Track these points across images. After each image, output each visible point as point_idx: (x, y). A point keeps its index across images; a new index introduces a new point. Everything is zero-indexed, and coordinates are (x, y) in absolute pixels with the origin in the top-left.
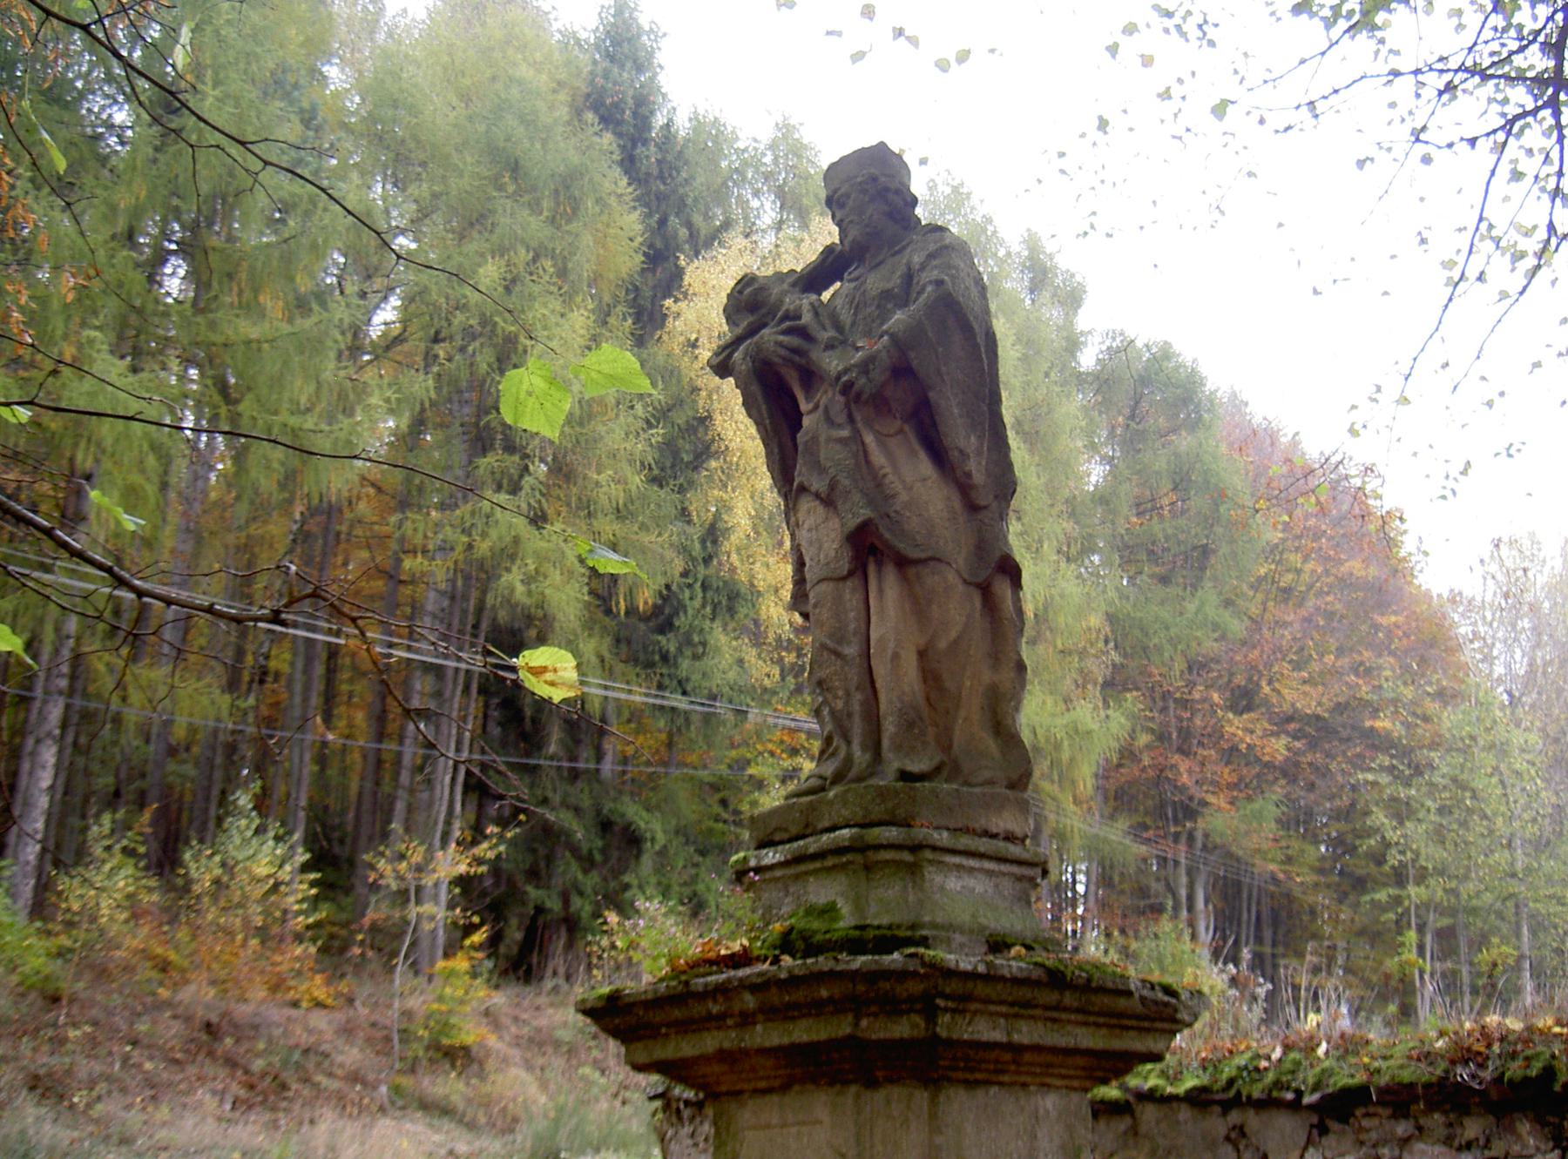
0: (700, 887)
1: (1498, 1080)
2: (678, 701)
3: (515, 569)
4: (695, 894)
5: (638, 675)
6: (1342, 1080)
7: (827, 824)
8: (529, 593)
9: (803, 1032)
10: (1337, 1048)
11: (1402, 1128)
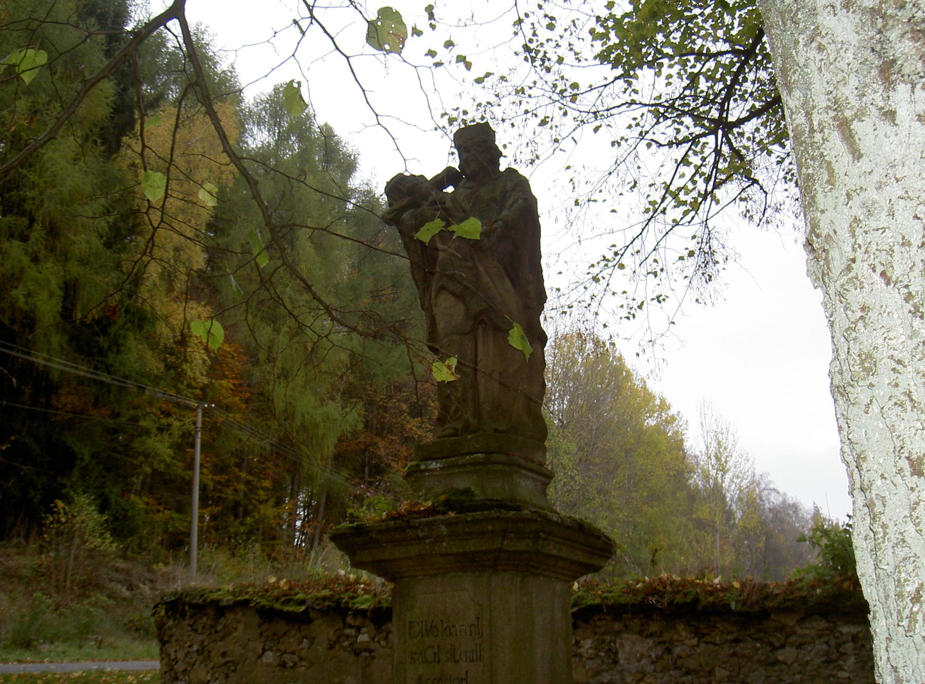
0: (106, 490)
1: (671, 603)
2: (106, 378)
3: (20, 287)
4: (103, 494)
5: (83, 360)
6: (590, 600)
7: (466, 451)
8: (26, 303)
9: (472, 546)
10: (583, 586)
11: (617, 626)
